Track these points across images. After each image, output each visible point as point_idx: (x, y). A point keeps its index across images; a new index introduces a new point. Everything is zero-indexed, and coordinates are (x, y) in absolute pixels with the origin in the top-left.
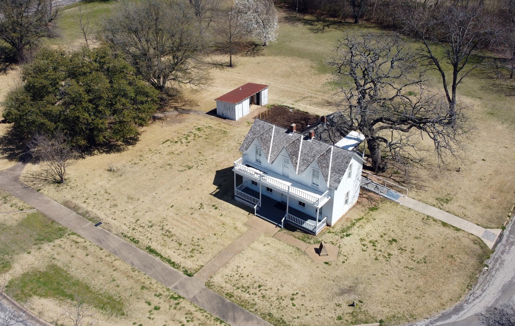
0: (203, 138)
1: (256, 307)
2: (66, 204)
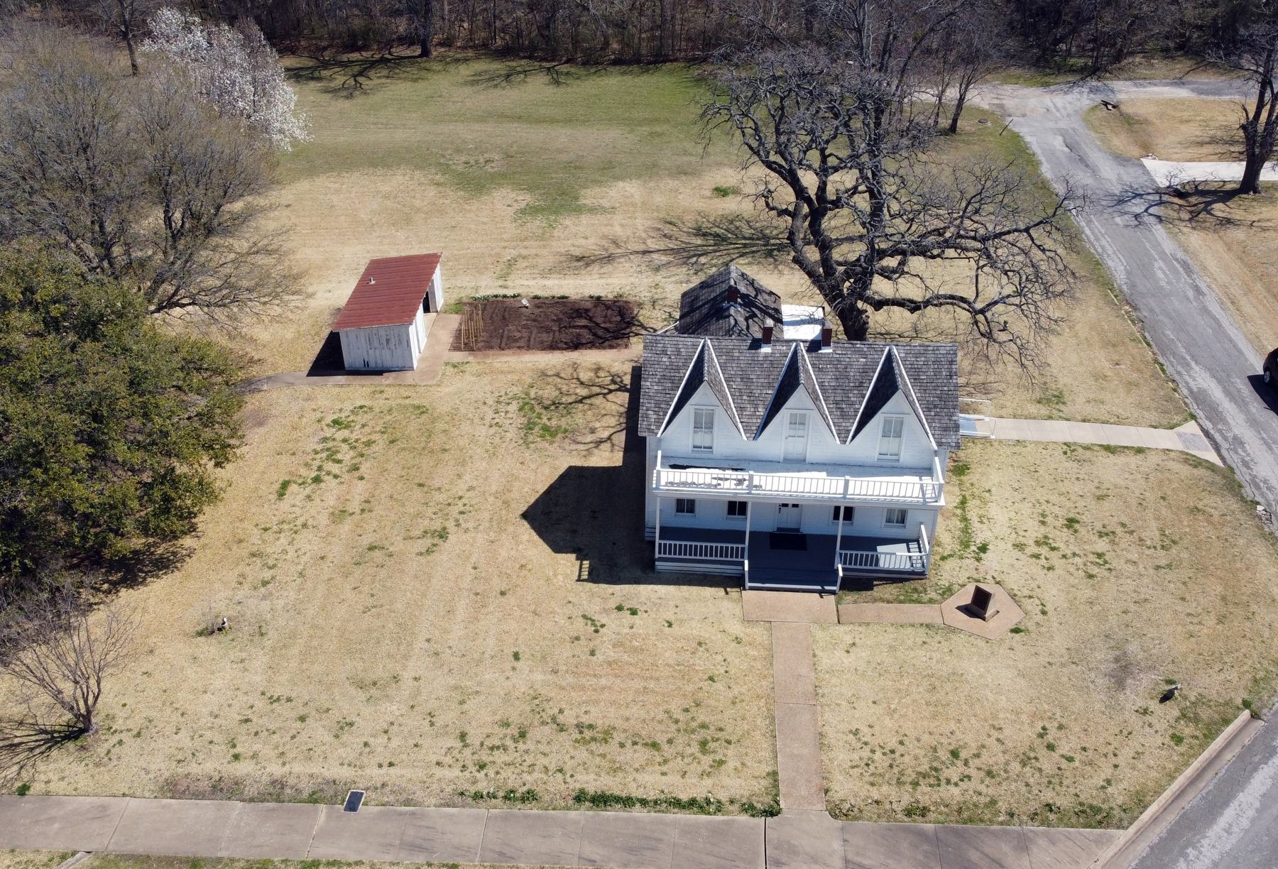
0: (1107, 407)
1: (1003, 806)
2: (172, 788)
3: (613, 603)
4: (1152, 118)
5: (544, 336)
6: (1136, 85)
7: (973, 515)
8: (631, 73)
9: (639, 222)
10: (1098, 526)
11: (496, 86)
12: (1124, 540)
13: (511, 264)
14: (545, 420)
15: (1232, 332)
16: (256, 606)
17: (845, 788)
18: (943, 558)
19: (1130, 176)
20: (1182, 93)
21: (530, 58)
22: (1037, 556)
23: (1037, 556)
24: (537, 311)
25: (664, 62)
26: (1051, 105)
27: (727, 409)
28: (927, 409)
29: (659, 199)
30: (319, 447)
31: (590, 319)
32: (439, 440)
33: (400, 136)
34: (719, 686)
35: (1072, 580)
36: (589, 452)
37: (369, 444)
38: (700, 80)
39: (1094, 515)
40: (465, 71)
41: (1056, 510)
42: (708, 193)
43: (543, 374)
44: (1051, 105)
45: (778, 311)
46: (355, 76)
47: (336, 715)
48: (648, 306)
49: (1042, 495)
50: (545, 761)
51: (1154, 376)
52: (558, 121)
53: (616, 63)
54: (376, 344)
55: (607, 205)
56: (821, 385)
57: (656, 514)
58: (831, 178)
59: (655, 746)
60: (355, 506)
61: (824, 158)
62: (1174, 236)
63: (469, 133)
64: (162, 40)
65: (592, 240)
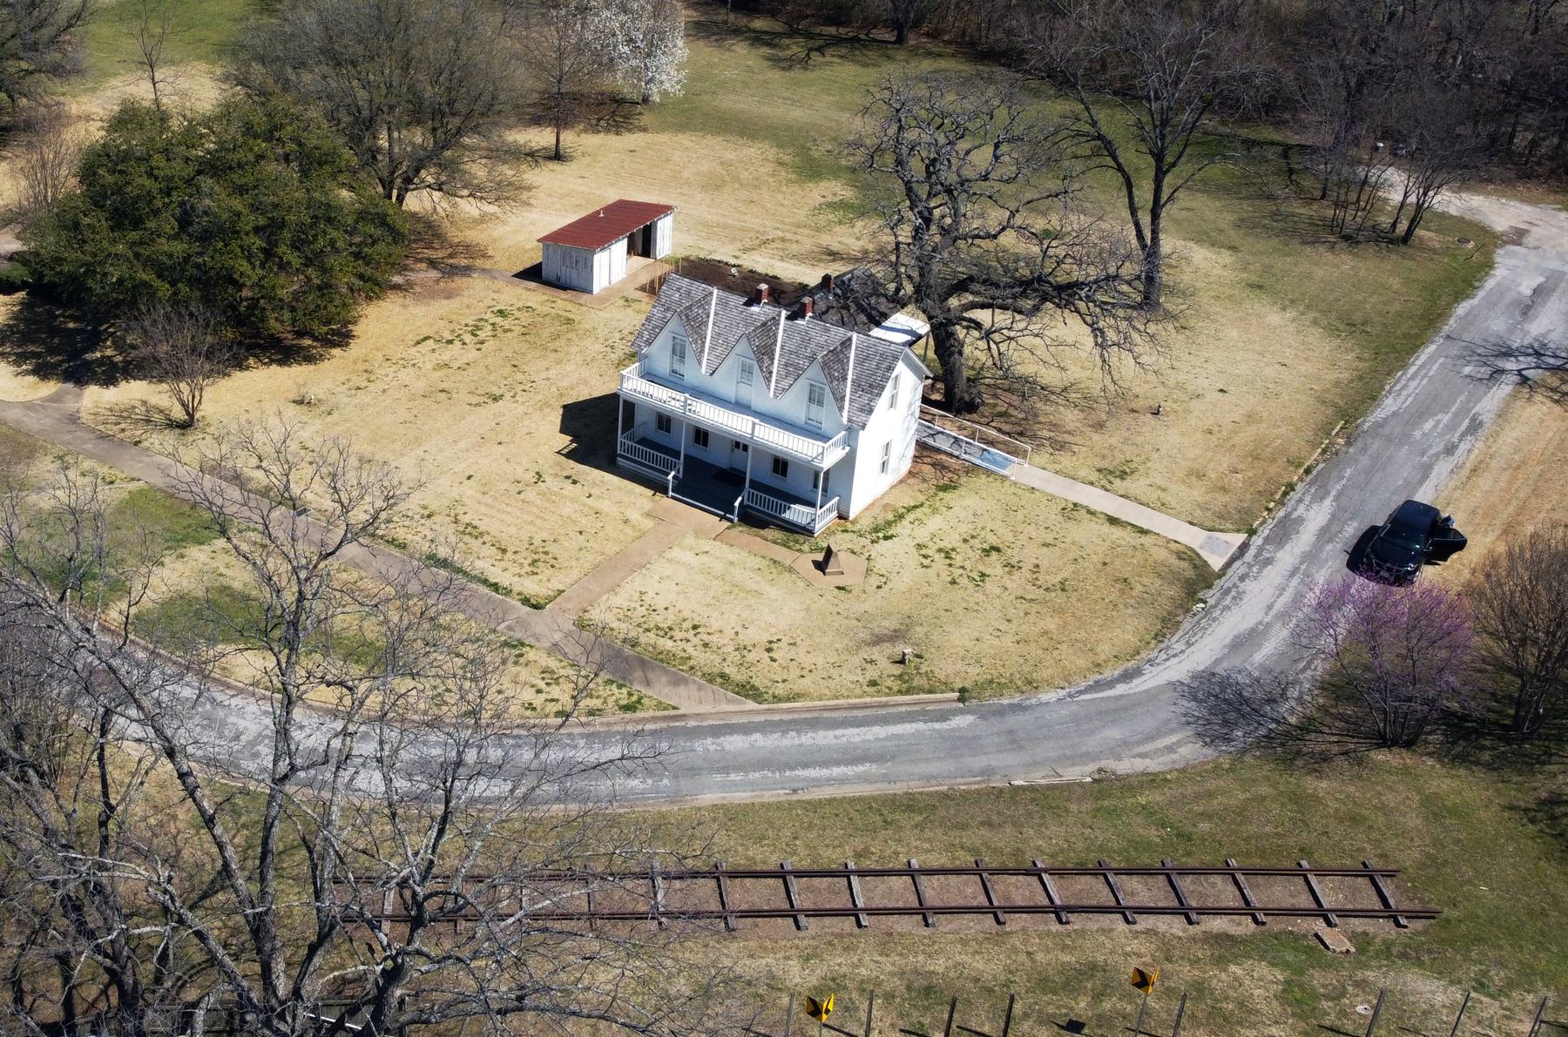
1: (692, 663)
54: (568, 262)
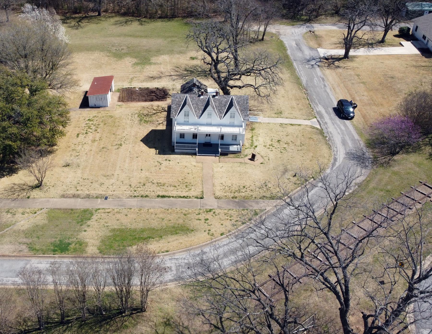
1: (254, 196)
3: (164, 159)
4: (323, 36)
5: (143, 98)
6: (321, 25)
7: (254, 139)
8: (165, 21)
9: (168, 67)
10: (285, 142)
11: (122, 25)
12: (291, 144)
13: (132, 79)
14: (145, 119)
15: (332, 97)
16: (76, 161)
17: (218, 194)
18: (246, 149)
19: (313, 54)
20: (334, 28)
21: (133, 16)
22: (269, 148)
23: (269, 148)
24: (140, 92)
25: (175, 17)
26: (294, 32)
27: (192, 111)
28: (241, 111)
29: (174, 61)
30: (86, 126)
31: (156, 94)
32: (117, 124)
33: (94, 41)
34: (190, 175)
35: (277, 153)
36: (157, 126)
37: (99, 125)
38: (186, 24)
39: (285, 139)
40: (112, 20)
41: (275, 138)
42: (188, 59)
43: (144, 107)
44: (294, 32)
45: (206, 90)
46: (78, 22)
47: (99, 182)
48: (172, 90)
49: (272, 135)
50: (150, 190)
51: (308, 107)
52: (143, 37)
53: (160, 18)
54: (98, 100)
55: (159, 62)
56: (215, 106)
57: (175, 138)
58: (220, 55)
59: (175, 186)
60: (97, 139)
61: (218, 49)
62: (321, 70)
63: (116, 40)
64: (27, 13)
65: (155, 72)
